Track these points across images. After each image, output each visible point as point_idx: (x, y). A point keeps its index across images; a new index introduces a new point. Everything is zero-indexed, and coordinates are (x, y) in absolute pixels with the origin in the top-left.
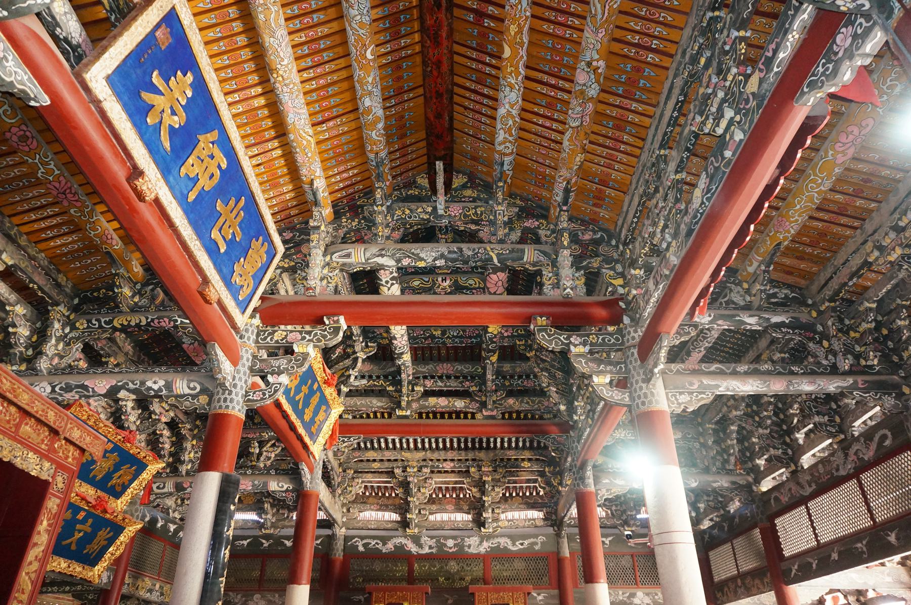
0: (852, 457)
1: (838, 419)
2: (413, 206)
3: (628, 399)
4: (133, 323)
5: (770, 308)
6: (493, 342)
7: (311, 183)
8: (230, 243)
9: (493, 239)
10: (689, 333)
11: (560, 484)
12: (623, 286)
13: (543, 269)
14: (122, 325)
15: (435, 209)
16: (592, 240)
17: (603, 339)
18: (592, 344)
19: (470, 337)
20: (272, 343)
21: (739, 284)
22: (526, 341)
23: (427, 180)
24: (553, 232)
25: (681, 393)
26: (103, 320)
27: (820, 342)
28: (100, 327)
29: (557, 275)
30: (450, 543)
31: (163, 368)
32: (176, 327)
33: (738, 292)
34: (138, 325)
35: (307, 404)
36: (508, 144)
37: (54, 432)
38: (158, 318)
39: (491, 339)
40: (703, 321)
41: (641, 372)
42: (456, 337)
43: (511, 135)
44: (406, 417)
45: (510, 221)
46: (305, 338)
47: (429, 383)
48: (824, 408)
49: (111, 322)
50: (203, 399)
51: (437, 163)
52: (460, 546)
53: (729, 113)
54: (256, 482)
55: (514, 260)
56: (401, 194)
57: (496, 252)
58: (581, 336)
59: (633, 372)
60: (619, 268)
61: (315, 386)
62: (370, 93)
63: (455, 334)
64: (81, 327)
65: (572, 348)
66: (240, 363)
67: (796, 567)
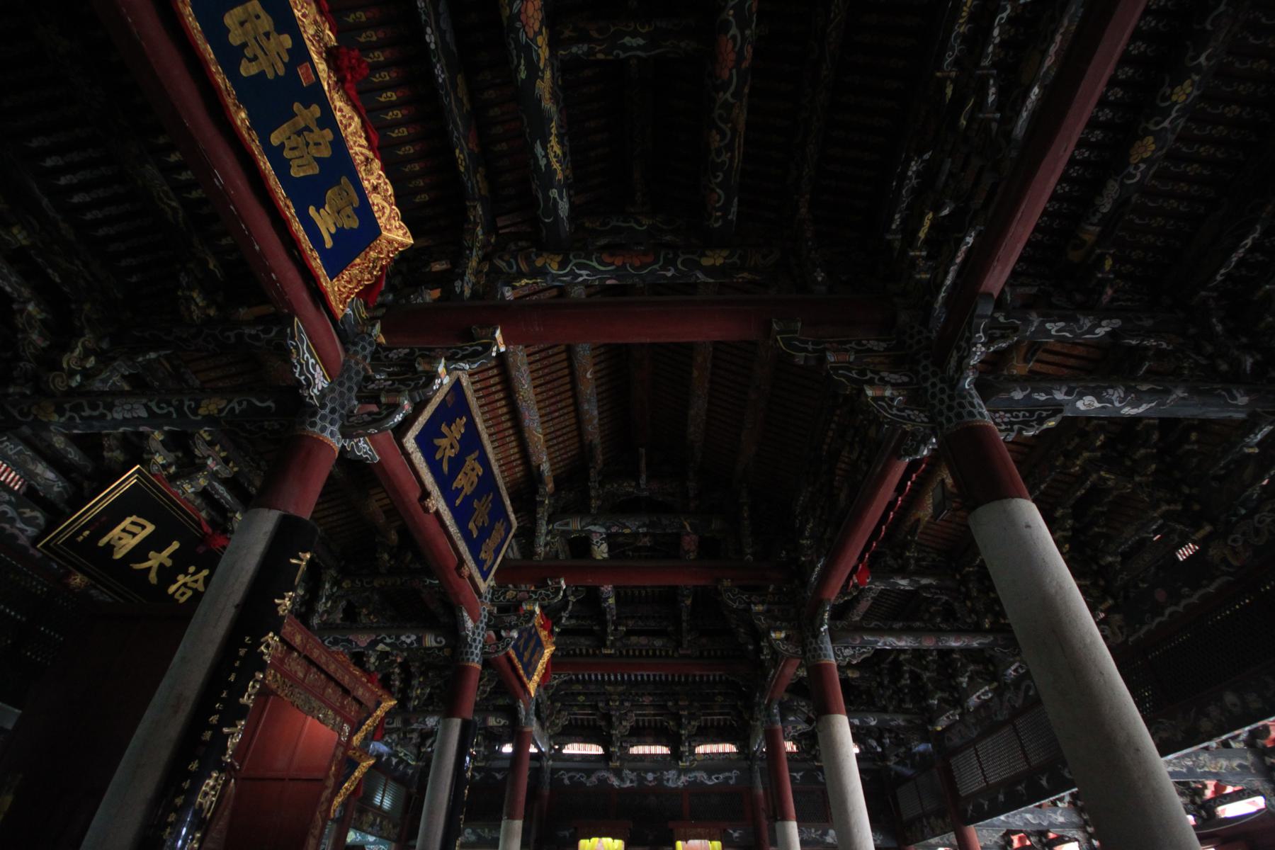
7: (539, 467)
8: (480, 530)
11: (751, 718)
15: (638, 484)
20: (504, 602)
30: (650, 776)
35: (525, 648)
37: (346, 692)
47: (630, 623)
52: (659, 780)
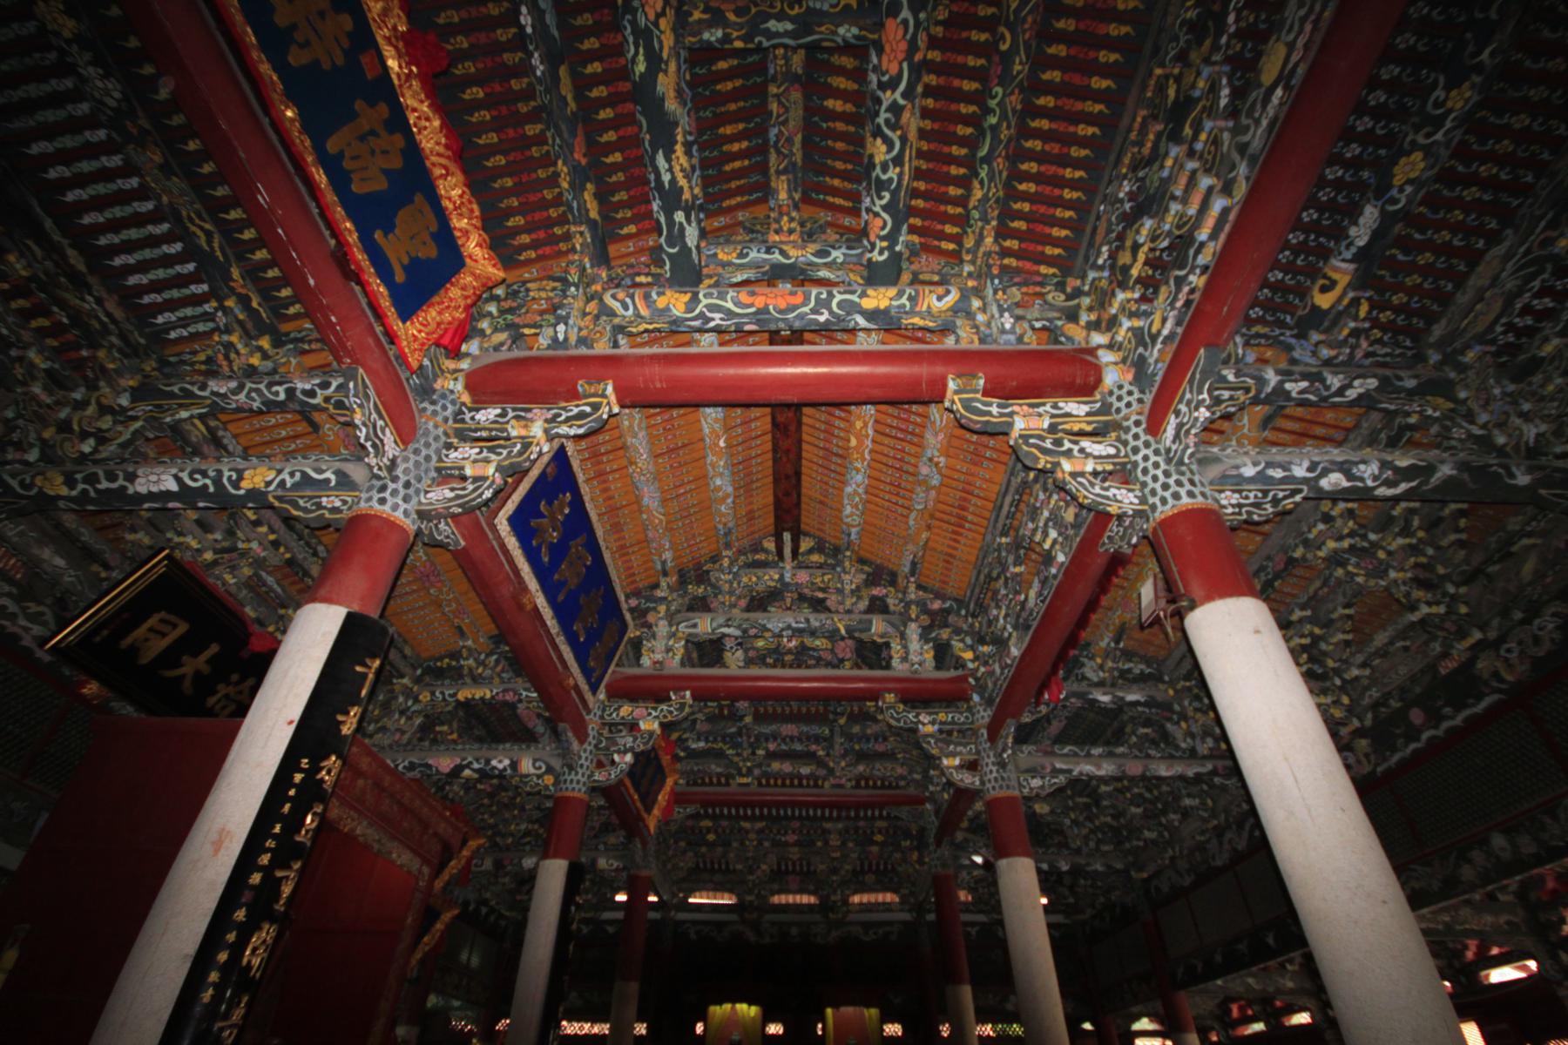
0: (1226, 846)
1: (1209, 802)
2: (760, 572)
9: (841, 609)
15: (782, 576)
18: (941, 723)
21: (1092, 659)
24: (901, 601)
27: (1177, 723)
29: (905, 647)
31: (508, 745)
34: (482, 699)
44: (747, 785)
45: (858, 588)
48: (1194, 790)
49: (455, 695)
50: (549, 780)
53: (1053, 534)
55: (861, 631)
58: (930, 714)
60: (969, 641)
62: (721, 475)
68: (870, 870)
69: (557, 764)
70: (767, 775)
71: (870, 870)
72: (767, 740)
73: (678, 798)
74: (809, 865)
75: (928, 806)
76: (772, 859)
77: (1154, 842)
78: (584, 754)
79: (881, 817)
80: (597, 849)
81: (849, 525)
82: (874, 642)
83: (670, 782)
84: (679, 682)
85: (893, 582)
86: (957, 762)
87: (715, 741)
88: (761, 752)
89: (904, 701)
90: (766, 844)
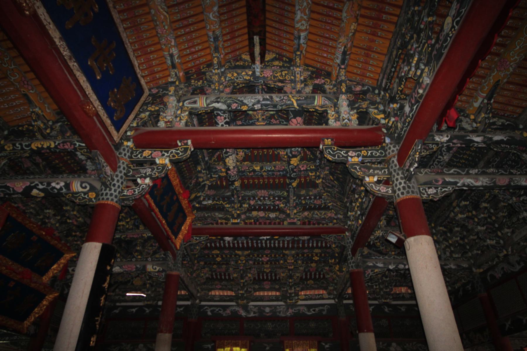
2: (239, 71)
3: (390, 192)
4: (45, 146)
5: (492, 132)
6: (294, 172)
10: (432, 148)
12: (385, 119)
13: (328, 109)
14: (37, 147)
15: (254, 72)
16: (361, 91)
17: (371, 153)
18: (363, 157)
19: (279, 171)
21: (468, 116)
22: (316, 173)
23: (249, 57)
25: (429, 188)
26: (24, 144)
28: (22, 149)
32: (75, 149)
33: (467, 122)
34: (49, 148)
36: (303, 22)
38: (63, 143)
39: (292, 169)
40: (442, 140)
41: (400, 173)
42: (270, 171)
43: (305, 15)
46: (164, 155)
50: (92, 195)
51: (255, 37)
54: (138, 266)
56: (231, 64)
57: (296, 98)
58: (356, 151)
59: (393, 173)
60: (381, 107)
61: (175, 198)
63: (269, 169)
64: (8, 149)
65: (349, 158)
66: (118, 170)
67: (509, 323)
68: (311, 278)
69: (98, 185)
70: (249, 218)
71: (311, 278)
72: (249, 199)
73: (194, 232)
74: (276, 276)
75: (347, 234)
76: (254, 271)
77: (493, 246)
78: (118, 180)
79: (317, 247)
80: (147, 260)
81: (300, 31)
82: (316, 111)
83: (189, 220)
84: (183, 134)
85: (328, 75)
86: (375, 179)
87: (219, 200)
88: (246, 206)
89: (336, 144)
90: (251, 262)
